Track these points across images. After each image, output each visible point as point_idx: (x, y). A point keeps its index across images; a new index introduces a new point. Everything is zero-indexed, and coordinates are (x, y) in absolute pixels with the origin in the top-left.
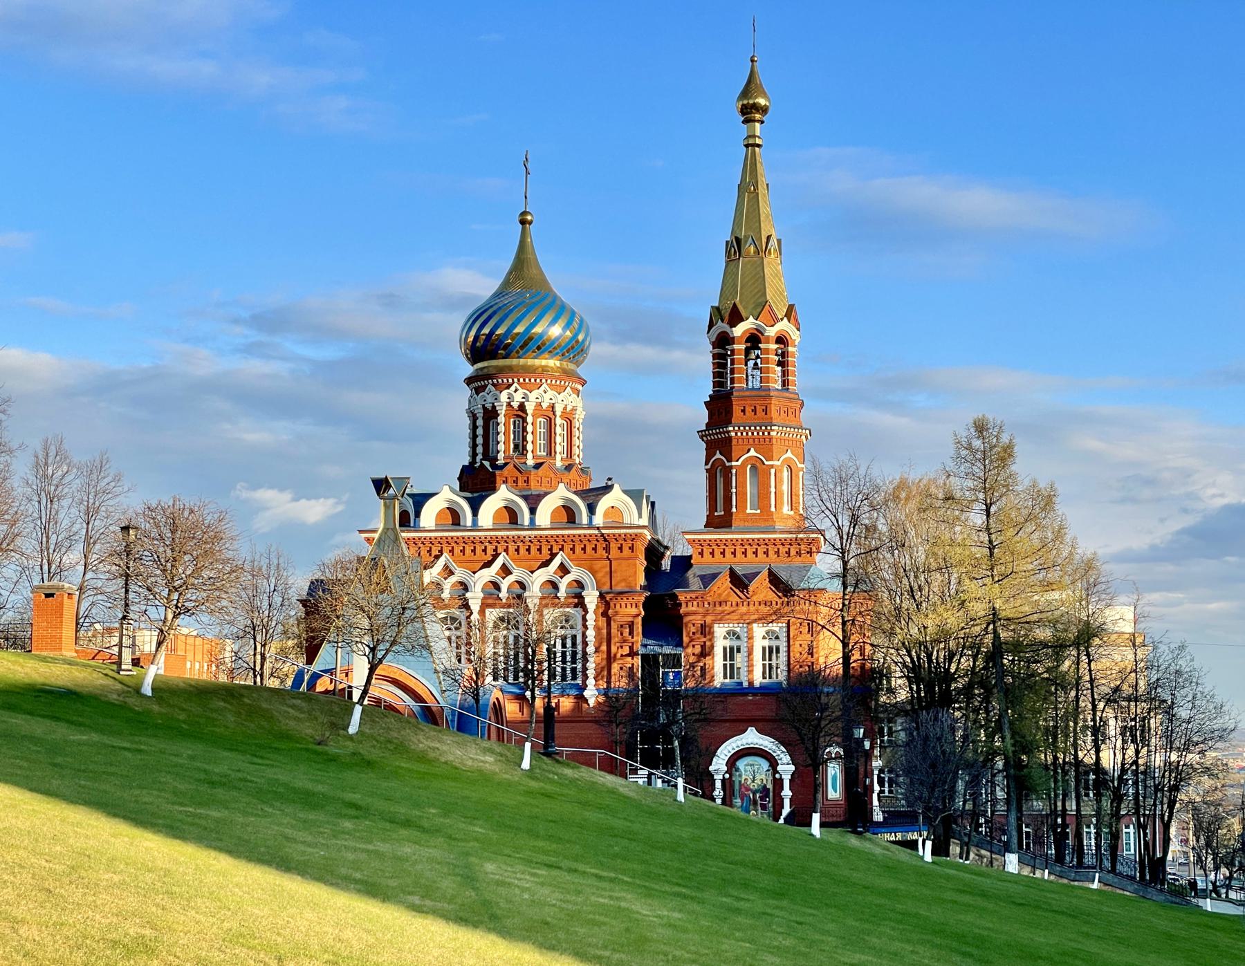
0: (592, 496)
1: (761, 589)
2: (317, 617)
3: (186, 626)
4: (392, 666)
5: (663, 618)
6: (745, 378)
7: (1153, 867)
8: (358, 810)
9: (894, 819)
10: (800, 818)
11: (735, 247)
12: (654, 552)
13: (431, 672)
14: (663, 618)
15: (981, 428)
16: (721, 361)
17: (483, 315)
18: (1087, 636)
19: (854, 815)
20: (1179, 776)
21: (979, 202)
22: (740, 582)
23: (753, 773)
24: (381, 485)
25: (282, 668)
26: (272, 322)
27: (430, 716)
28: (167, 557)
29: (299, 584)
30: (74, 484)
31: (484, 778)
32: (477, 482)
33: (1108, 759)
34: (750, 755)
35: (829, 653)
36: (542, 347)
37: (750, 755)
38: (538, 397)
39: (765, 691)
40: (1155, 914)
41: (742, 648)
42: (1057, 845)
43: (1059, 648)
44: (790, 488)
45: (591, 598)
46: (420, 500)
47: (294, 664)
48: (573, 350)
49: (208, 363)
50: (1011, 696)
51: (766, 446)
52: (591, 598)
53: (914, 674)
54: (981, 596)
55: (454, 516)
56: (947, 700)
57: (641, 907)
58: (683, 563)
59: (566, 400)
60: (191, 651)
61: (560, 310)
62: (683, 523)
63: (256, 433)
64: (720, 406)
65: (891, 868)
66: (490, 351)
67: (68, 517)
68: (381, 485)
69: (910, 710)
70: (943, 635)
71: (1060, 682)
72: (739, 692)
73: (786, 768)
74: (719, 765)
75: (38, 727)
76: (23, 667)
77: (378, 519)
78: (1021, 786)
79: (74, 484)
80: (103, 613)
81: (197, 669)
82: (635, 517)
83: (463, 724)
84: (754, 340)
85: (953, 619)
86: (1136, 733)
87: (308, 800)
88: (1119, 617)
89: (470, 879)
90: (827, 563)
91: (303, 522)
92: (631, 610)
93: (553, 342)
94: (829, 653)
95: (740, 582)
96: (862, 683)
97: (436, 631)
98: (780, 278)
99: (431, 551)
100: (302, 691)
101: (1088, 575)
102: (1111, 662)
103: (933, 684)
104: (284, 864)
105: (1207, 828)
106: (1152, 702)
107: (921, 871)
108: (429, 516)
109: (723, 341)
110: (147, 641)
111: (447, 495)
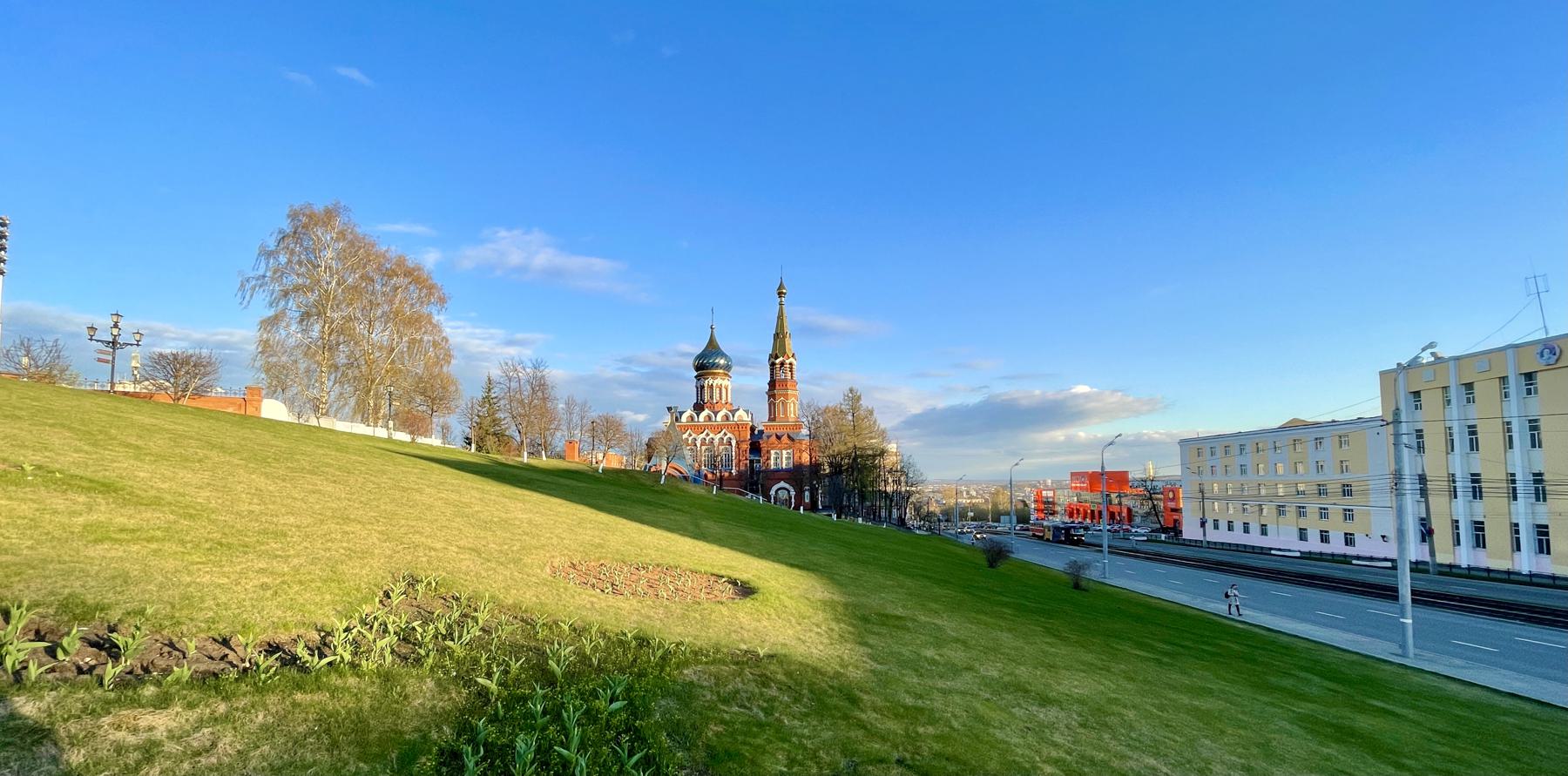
0: (733, 412)
1: (785, 439)
2: (651, 449)
3: (611, 452)
4: (673, 464)
5: (755, 448)
6: (780, 375)
7: (902, 522)
8: (665, 506)
9: (825, 508)
10: (797, 508)
11: (776, 336)
12: (753, 429)
13: (685, 466)
14: (755, 448)
15: (851, 390)
16: (772, 370)
17: (699, 357)
18: (883, 453)
19: (813, 507)
20: (910, 494)
21: (839, 323)
22: (778, 438)
23: (783, 495)
24: (669, 409)
25: (640, 464)
26: (628, 361)
27: (686, 478)
28: (606, 430)
29: (646, 440)
30: (577, 409)
31: (701, 497)
32: (699, 407)
33: (889, 489)
34: (782, 490)
35: (806, 458)
36: (718, 366)
37: (782, 490)
38: (718, 381)
39: (787, 471)
40: (902, 534)
41: (780, 458)
42: (872, 515)
43: (874, 456)
44: (793, 410)
45: (734, 443)
46: (681, 413)
47: (644, 463)
48: (728, 368)
49: (610, 373)
50: (860, 471)
51: (786, 396)
52: (734, 443)
53: (831, 464)
54: (852, 441)
55: (692, 418)
56: (841, 472)
57: (748, 534)
58: (761, 432)
59: (725, 382)
60: (613, 459)
61: (723, 355)
62: (761, 420)
63: (626, 394)
64: (772, 384)
65: (823, 522)
66: (704, 366)
67: (576, 418)
68: (669, 409)
69: (830, 475)
70: (839, 453)
71: (875, 467)
72: (777, 471)
73: (793, 493)
74: (773, 492)
75: (568, 482)
76: (135, 730)
77: (668, 419)
78: (863, 498)
79: (577, 409)
80: (586, 447)
81: (615, 465)
82: (747, 418)
83: (695, 481)
84: (782, 364)
85: (843, 448)
86: (897, 482)
87: (648, 503)
88: (892, 447)
89: (697, 526)
90: (805, 431)
91: (644, 420)
92: (746, 446)
93: (627, 429)
94: (806, 458)
95: (778, 438)
96: (815, 467)
97: (687, 453)
98: (790, 345)
99: (686, 428)
100: (646, 472)
101: (883, 434)
102: (889, 461)
103: (837, 469)
104: (642, 522)
105: (917, 509)
106: (901, 472)
107: (833, 522)
108: (684, 418)
109: (773, 365)
110: (600, 457)
111: (689, 412)
